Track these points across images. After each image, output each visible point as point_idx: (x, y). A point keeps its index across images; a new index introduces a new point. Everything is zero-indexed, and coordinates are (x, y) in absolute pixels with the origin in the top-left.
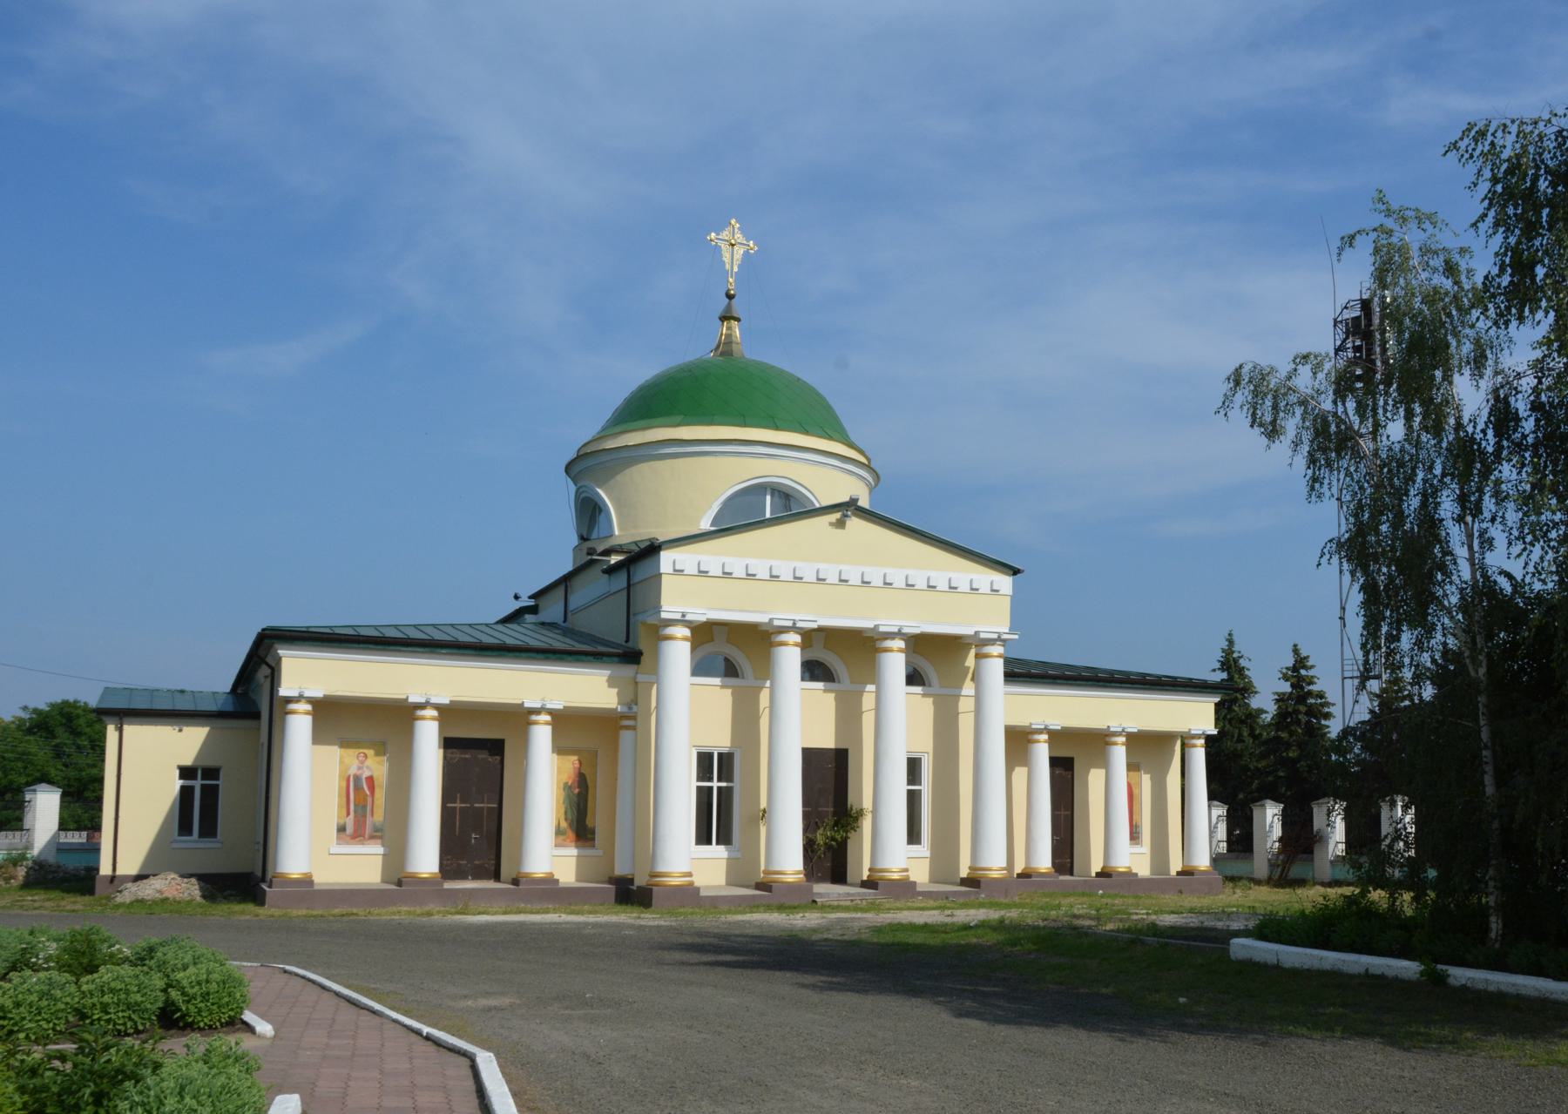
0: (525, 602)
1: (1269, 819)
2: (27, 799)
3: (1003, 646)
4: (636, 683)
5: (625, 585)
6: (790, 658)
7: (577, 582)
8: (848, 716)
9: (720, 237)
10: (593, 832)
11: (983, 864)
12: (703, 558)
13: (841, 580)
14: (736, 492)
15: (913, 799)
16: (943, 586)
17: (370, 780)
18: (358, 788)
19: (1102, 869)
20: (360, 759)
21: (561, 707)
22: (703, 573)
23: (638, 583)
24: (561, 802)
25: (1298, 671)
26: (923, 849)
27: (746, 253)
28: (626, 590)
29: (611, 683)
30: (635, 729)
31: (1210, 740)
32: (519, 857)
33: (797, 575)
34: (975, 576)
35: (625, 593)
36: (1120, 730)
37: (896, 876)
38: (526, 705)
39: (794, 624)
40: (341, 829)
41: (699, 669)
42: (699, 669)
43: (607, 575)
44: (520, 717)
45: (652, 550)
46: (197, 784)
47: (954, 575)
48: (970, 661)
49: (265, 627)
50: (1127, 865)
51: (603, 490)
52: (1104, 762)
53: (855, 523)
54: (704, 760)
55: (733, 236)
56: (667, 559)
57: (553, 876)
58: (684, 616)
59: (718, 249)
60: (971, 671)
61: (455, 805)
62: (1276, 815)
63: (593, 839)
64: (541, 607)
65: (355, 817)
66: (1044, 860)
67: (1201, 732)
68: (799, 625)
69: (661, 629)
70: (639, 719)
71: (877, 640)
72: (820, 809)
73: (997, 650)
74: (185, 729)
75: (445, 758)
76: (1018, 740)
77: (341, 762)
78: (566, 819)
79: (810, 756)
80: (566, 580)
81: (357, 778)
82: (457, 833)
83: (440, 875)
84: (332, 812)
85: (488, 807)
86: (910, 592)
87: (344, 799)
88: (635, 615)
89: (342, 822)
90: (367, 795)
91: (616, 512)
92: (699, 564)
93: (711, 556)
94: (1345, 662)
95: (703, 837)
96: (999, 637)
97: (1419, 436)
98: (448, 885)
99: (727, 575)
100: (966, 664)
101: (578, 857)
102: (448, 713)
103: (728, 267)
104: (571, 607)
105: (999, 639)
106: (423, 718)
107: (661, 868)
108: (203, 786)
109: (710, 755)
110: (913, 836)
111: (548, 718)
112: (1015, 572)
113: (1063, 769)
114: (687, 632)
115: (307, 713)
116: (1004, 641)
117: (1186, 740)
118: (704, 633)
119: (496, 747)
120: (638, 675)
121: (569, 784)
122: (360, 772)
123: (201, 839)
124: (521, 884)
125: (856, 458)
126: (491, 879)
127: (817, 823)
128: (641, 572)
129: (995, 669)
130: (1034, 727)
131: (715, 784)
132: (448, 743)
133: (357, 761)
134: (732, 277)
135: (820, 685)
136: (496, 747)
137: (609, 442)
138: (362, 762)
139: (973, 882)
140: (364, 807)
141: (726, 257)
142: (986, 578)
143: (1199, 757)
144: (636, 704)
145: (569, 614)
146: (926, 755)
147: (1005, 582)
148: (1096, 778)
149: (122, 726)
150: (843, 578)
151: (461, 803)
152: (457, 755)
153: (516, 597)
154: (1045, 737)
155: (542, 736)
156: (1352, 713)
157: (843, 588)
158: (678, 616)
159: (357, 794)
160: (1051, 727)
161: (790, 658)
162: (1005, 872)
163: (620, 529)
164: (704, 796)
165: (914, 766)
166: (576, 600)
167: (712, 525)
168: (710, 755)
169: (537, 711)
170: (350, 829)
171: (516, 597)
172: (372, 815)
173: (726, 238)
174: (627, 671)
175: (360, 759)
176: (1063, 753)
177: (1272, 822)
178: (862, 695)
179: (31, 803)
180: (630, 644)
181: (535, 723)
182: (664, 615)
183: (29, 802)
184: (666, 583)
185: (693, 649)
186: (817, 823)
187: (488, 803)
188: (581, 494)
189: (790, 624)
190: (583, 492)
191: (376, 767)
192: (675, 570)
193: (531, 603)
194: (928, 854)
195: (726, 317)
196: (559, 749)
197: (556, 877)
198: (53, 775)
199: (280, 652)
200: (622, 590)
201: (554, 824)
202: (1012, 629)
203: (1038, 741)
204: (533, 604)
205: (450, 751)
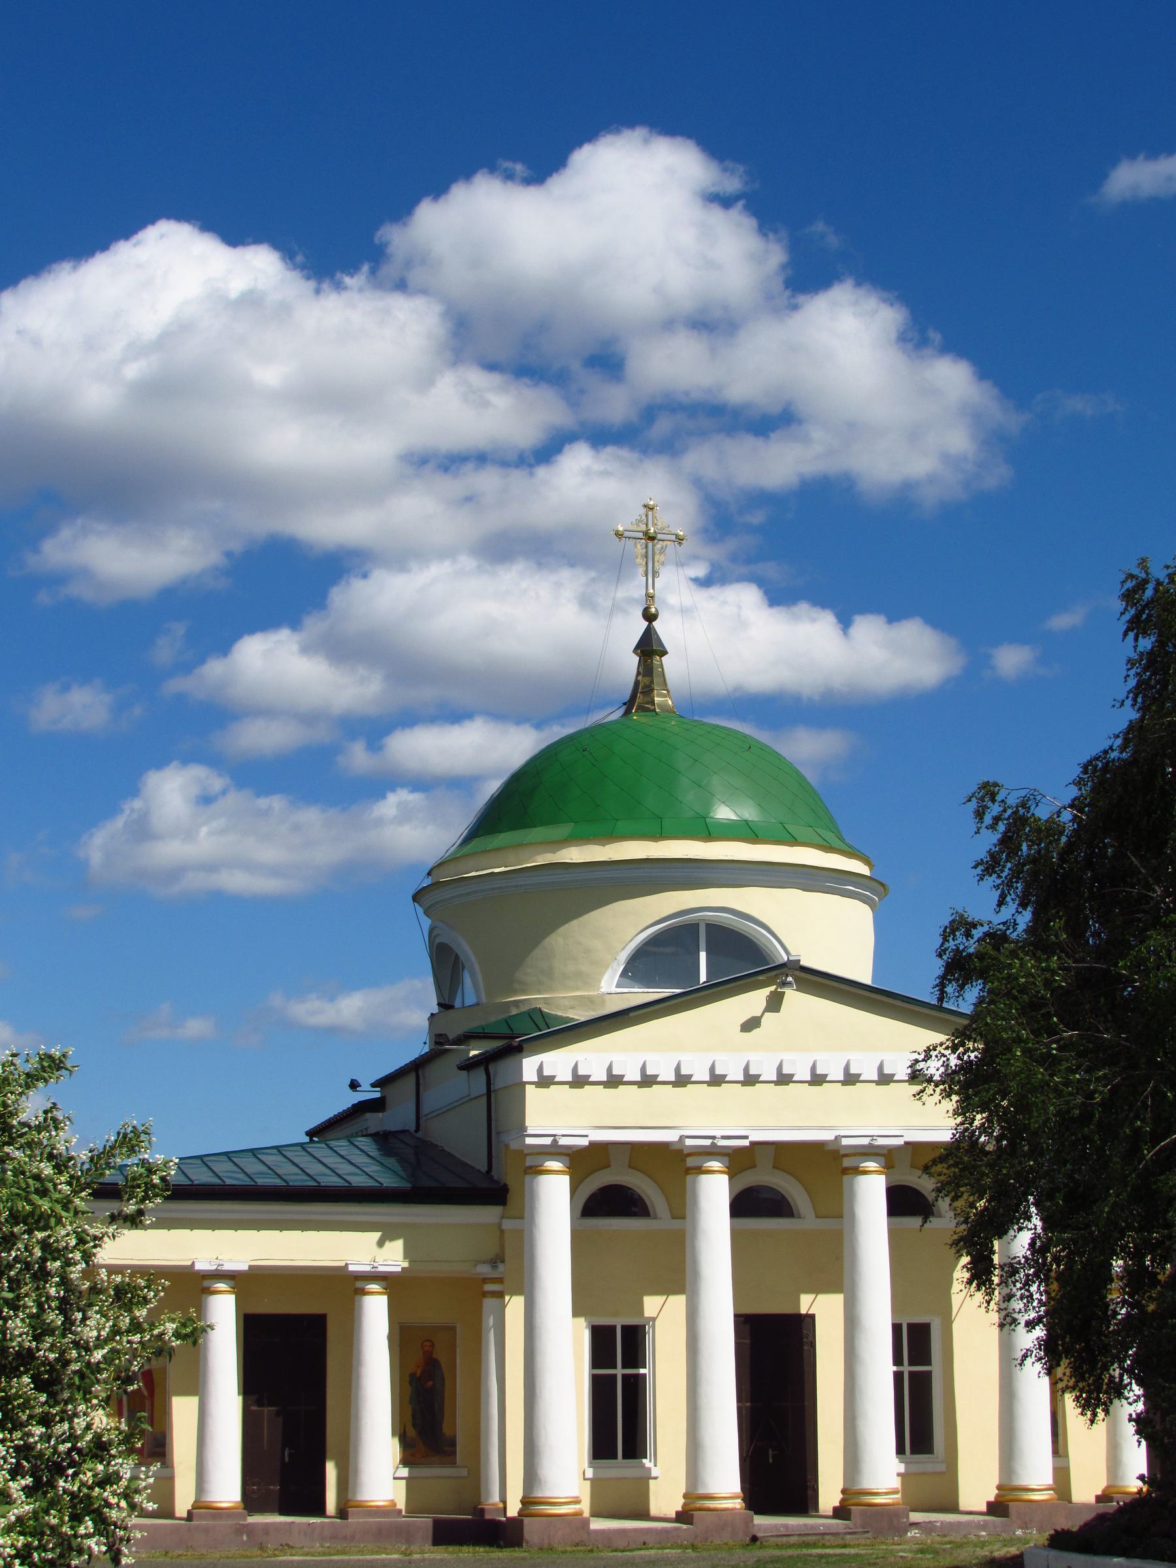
0: (368, 1093)
4: (502, 1232)
5: (484, 1091)
7: (434, 1070)
10: (453, 1443)
19: (1104, 1491)
25: (8, 1530)
28: (485, 1096)
35: (484, 1100)
43: (464, 1073)
57: (395, 1505)
63: (454, 1453)
64: (389, 1101)
78: (414, 1425)
80: (417, 1067)
82: (265, 1448)
83: (242, 1505)
97: (61, 1519)
98: (252, 1519)
101: (409, 1480)
102: (243, 1283)
104: (426, 1109)
121: (418, 1374)
124: (194, 1519)
126: (274, 1512)
128: (501, 1069)
131: (619, 1371)
144: (503, 1261)
145: (422, 1121)
153: (354, 1085)
162: (1052, 1492)
167: (618, 986)
190: (437, 936)
193: (376, 1094)
198: (15, 1496)
204: (378, 1095)
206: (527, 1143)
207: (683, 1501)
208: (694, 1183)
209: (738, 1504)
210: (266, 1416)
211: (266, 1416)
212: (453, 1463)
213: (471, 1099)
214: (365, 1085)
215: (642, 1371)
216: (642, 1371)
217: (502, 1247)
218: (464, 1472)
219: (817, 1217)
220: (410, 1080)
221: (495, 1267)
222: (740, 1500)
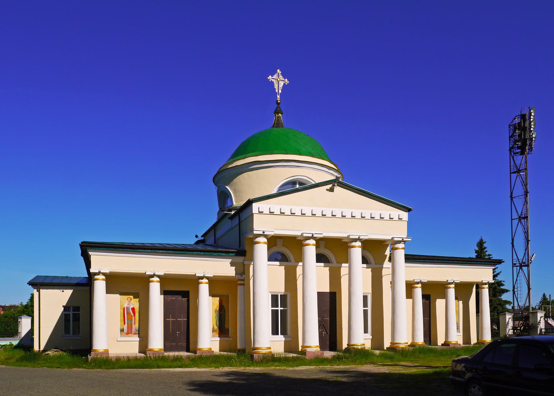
0: (200, 238)
1: (539, 319)
2: (19, 321)
3: (404, 244)
4: (244, 265)
5: (238, 222)
6: (311, 252)
8: (335, 278)
9: (273, 78)
11: (397, 341)
12: (271, 206)
13: (332, 216)
14: (284, 183)
15: (365, 312)
16: (378, 217)
17: (133, 309)
18: (128, 313)
20: (129, 300)
21: (212, 276)
22: (271, 213)
23: (243, 220)
24: (214, 317)
26: (369, 336)
27: (284, 84)
29: (232, 264)
30: (244, 285)
31: (491, 286)
32: (196, 342)
33: (313, 213)
34: (392, 213)
36: (452, 281)
37: (360, 348)
38: (197, 275)
39: (313, 235)
40: (122, 330)
41: (271, 258)
42: (271, 258)
43: (230, 220)
44: (195, 281)
45: (249, 203)
46: (71, 313)
47: (382, 212)
48: (388, 253)
49: (82, 241)
50: (456, 341)
51: (229, 187)
52: (444, 296)
53: (337, 189)
54: (274, 298)
55: (279, 77)
56: (255, 206)
58: (264, 232)
59: (272, 83)
60: (388, 257)
61: (170, 320)
62: (511, 318)
65: (128, 325)
66: (420, 339)
67: (487, 282)
68: (315, 236)
69: (254, 239)
70: (245, 281)
71: (349, 242)
72: (324, 319)
73: (401, 245)
74: (65, 290)
75: (164, 299)
76: (410, 287)
77: (121, 302)
78: (216, 325)
79: (320, 295)
80: (214, 226)
81: (128, 308)
84: (117, 323)
85: (183, 320)
86: (363, 220)
87: (123, 318)
88: (242, 235)
89: (122, 328)
90: (132, 316)
91: (233, 194)
92: (270, 209)
93: (275, 205)
94: (514, 260)
95: (275, 332)
96: (403, 240)
99: (282, 213)
100: (385, 254)
101: (220, 341)
102: (164, 280)
103: (277, 91)
104: (217, 237)
105: (403, 241)
106: (153, 281)
107: (257, 346)
108: (73, 314)
109: (277, 296)
110: (366, 331)
111: (207, 281)
112: (408, 210)
113: (426, 297)
114: (265, 240)
115: (103, 280)
116: (405, 242)
117: (479, 286)
118: (273, 241)
119: (185, 294)
120: (245, 261)
122: (129, 305)
123: (74, 335)
125: (333, 167)
127: (323, 325)
128: (244, 215)
129: (400, 255)
130: (415, 281)
131: (279, 309)
132: (165, 292)
133: (127, 301)
134: (278, 95)
135: (322, 264)
136: (185, 294)
137: (230, 166)
138: (130, 302)
139: (393, 348)
140: (131, 320)
141: (276, 86)
142: (396, 213)
143: (486, 293)
144: (244, 274)
146: (369, 294)
147: (405, 215)
148: (440, 304)
149: (39, 290)
150: (333, 214)
151: (172, 319)
152: (170, 298)
153: (197, 236)
154: (420, 285)
155: (204, 288)
156: (517, 280)
157: (334, 219)
158: (261, 233)
159: (127, 314)
160: (423, 281)
161: (311, 252)
163: (236, 202)
164: (275, 314)
165: (365, 298)
166: (219, 233)
168: (277, 296)
169: (202, 278)
170: (126, 331)
171: (197, 236)
172: (135, 324)
173: (276, 78)
174: (240, 259)
175: (129, 300)
176: (427, 293)
177: (540, 320)
178: (341, 268)
179: (20, 323)
180: (241, 248)
181: (201, 283)
182: (255, 232)
183: (20, 322)
184: (255, 216)
185: (269, 249)
186: (323, 325)
187: (183, 319)
188: (219, 190)
189: (311, 235)
191: (135, 303)
192: (259, 212)
193: (203, 238)
194: (371, 337)
195: (276, 112)
196: (212, 294)
197: (212, 350)
199: (90, 253)
200: (237, 225)
201: (212, 327)
202: (408, 236)
203: (417, 287)
205: (166, 296)
206: (254, 233)
207: (347, 346)
208: (304, 248)
209: (319, 349)
210: (171, 317)
211: (171, 317)
212: (228, 337)
213: (233, 228)
214: (200, 236)
215: (282, 309)
216: (282, 309)
217: (244, 270)
218: (232, 339)
219: (337, 263)
220: (213, 231)
221: (242, 276)
222: (319, 348)
